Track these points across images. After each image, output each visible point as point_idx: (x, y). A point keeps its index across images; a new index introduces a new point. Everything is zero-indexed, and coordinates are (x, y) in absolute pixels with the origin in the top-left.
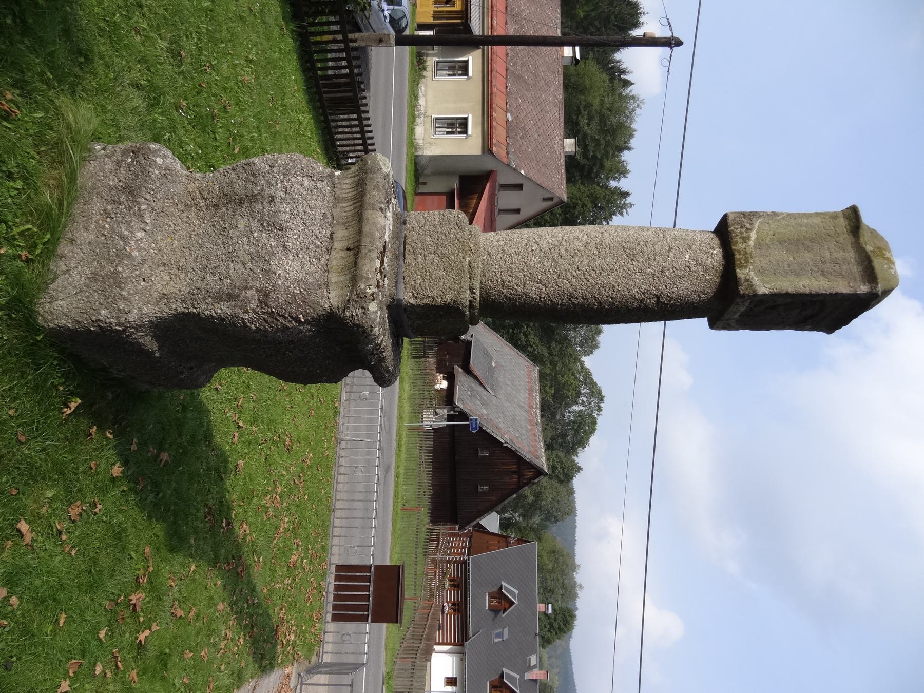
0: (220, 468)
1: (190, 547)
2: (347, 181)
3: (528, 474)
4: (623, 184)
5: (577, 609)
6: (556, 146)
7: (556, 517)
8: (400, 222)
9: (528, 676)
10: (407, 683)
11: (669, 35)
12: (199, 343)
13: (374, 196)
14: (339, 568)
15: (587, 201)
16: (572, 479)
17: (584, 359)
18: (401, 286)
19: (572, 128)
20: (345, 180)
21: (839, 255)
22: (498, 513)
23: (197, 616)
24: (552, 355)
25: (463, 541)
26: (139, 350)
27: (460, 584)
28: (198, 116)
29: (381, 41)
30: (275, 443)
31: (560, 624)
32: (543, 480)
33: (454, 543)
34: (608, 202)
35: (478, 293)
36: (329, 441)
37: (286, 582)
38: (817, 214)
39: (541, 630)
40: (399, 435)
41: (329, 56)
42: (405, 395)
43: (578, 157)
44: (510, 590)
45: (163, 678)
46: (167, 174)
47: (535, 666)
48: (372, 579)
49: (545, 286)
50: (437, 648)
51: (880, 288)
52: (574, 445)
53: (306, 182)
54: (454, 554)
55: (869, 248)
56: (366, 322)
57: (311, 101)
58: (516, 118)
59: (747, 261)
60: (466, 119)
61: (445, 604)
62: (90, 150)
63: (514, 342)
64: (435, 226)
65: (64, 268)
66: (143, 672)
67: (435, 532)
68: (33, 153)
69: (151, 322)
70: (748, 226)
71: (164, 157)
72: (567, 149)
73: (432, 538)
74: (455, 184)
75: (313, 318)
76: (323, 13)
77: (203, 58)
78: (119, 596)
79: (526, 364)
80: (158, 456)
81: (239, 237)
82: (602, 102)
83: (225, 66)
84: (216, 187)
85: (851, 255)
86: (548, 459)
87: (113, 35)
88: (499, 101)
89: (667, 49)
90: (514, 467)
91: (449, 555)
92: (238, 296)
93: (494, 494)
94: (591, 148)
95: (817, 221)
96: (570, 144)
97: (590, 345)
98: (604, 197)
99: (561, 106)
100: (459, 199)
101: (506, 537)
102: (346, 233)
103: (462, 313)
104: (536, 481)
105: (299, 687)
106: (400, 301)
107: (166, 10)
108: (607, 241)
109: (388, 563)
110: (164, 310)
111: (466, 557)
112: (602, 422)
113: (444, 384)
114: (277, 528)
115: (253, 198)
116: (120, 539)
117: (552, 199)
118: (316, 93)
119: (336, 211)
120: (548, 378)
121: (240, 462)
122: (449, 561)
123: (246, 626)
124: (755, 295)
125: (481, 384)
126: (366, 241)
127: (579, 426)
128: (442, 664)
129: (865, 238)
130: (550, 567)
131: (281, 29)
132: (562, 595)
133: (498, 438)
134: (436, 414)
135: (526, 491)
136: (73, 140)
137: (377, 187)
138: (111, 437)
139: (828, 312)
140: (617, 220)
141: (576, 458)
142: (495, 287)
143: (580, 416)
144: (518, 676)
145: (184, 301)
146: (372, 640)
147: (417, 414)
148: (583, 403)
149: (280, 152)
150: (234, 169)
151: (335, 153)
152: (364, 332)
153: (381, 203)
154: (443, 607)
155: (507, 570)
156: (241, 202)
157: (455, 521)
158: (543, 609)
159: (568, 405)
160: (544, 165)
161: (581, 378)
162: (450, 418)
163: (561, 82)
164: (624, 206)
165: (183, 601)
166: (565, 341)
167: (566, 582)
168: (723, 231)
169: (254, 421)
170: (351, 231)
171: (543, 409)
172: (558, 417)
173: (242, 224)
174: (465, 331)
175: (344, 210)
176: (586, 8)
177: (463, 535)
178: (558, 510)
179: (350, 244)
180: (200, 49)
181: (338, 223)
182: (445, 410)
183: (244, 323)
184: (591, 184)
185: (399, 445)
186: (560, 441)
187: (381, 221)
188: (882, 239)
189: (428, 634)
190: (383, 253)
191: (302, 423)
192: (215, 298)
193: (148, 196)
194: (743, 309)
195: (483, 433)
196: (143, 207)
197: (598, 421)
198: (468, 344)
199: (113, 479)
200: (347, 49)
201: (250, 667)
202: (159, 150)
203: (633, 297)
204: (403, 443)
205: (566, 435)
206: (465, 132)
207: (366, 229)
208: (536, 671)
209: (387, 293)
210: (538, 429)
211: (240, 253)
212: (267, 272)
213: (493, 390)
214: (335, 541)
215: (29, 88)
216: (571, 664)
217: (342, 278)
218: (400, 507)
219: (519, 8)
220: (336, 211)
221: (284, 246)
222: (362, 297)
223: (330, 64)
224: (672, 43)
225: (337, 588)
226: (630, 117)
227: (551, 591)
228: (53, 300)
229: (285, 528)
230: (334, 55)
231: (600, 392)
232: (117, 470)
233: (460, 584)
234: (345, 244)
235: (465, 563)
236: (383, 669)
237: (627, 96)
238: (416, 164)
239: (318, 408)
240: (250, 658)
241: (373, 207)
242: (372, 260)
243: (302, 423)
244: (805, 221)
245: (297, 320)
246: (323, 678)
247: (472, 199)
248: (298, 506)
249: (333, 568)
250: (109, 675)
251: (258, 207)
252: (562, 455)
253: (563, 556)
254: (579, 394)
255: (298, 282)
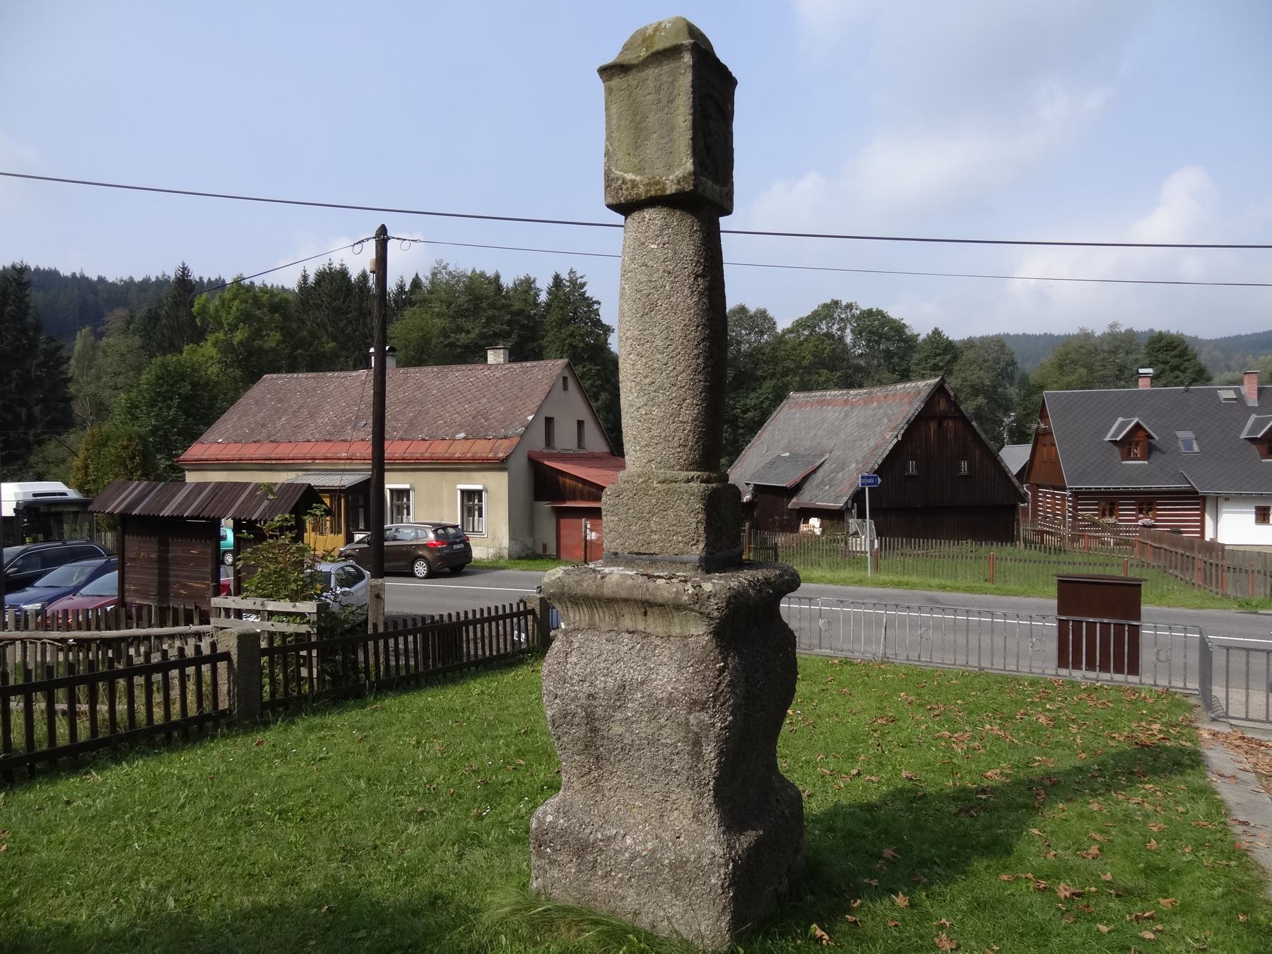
0: (912, 797)
1: (1007, 834)
2: (571, 615)
3: (943, 405)
4: (543, 284)
5: (1151, 330)
6: (498, 375)
7: (1008, 364)
8: (615, 558)
9: (1253, 401)
10: (1261, 577)
11: (373, 243)
12: (747, 783)
13: (588, 585)
14: (1062, 663)
15: (566, 332)
16: (951, 342)
17: (779, 330)
18: (685, 557)
19: (473, 354)
20: (566, 619)
21: (651, 84)
22: (1002, 446)
23: (1102, 832)
24: (774, 375)
25: (1044, 496)
26: (755, 851)
27: (1110, 502)
28: (487, 799)
29: (378, 596)
30: (883, 735)
31: (1172, 356)
32: (953, 383)
33: (1048, 510)
34: (567, 302)
35: (692, 473)
36: (885, 672)
37: (1075, 731)
38: (607, 109)
39: (1182, 384)
40: (884, 584)
41: (393, 663)
42: (829, 575)
43: (509, 345)
44: (1117, 429)
45: (1178, 873)
46: (561, 811)
47: (1238, 391)
48: (1077, 619)
49: (684, 400)
50: (1209, 536)
51: (687, 41)
52: (903, 341)
53: (573, 659)
54: (1063, 510)
55: (644, 53)
56: (724, 594)
57: (454, 682)
58: (461, 427)
59: (658, 183)
60: (463, 492)
61: (1140, 523)
62: (538, 894)
63: (755, 426)
64: (620, 520)
65: (666, 923)
66: (1164, 892)
67: (1030, 536)
68: (543, 947)
69: (724, 833)
70: (620, 182)
71: (545, 813)
72: (501, 360)
73: (1038, 541)
74: (546, 506)
75: (720, 653)
76: (356, 661)
77: (421, 790)
78: (1058, 909)
79: (785, 409)
80: (887, 860)
81: (632, 733)
82: (440, 315)
83: (428, 770)
84: (577, 758)
85: (651, 72)
86: (923, 377)
87: (412, 872)
88: (440, 449)
89: (390, 243)
90: (933, 426)
91: (1064, 517)
92: (696, 734)
93: (969, 451)
94: (498, 327)
95: (614, 109)
96: (495, 357)
97: (761, 321)
98: (562, 308)
99: (446, 369)
100: (564, 501)
101: (1037, 435)
102: (627, 617)
103: (715, 491)
104: (952, 394)
105: (1233, 722)
106: (701, 560)
107: (375, 823)
108: (637, 333)
109: (1055, 602)
110: (712, 817)
111: (1068, 493)
112: (865, 303)
113: (815, 522)
114: (998, 738)
115: (590, 717)
116: (986, 903)
117: (565, 379)
118: (444, 675)
119: (604, 627)
120: (807, 379)
121: (904, 774)
122: (1074, 517)
123: (1128, 780)
124: (695, 173)
125: (814, 471)
126: (637, 594)
127: (875, 334)
128: (1235, 528)
129: (631, 58)
130: (1083, 371)
131: (375, 710)
132: (1127, 353)
133: (891, 447)
134: (856, 534)
135: (968, 407)
136: (527, 909)
137: (578, 583)
138: (859, 901)
139: (713, 89)
140: (608, 315)
141: (921, 338)
142: (686, 455)
143: (860, 333)
144: (1254, 417)
145: (701, 795)
146: (1166, 625)
147: (856, 560)
148: (842, 329)
149: (540, 689)
150: (559, 738)
151: (514, 655)
152: (735, 597)
153: (595, 578)
154: (1144, 526)
155: (1087, 435)
156: (595, 730)
157: (1013, 508)
158: (1148, 381)
159: (845, 349)
160: (521, 389)
161: (806, 333)
162: (861, 515)
163: (417, 369)
164: (573, 282)
165: (1079, 848)
166: (755, 355)
167: (1106, 347)
168: (626, 208)
169: (852, 757)
170: (626, 610)
171: (850, 386)
172: (862, 363)
173: (617, 729)
174: (736, 492)
175: (603, 618)
176: (324, 339)
177: (1035, 497)
178: (997, 361)
179: (639, 611)
180: (412, 793)
181: (617, 625)
182: (851, 521)
183: (725, 728)
184: (548, 326)
185: (898, 585)
186: (896, 360)
187: (615, 578)
188: (633, 37)
189: (1184, 547)
190: (649, 577)
191: (857, 705)
192: (698, 759)
193: (588, 831)
194: (710, 183)
195: (882, 469)
196: (599, 836)
197: (865, 308)
198: (759, 489)
199: (912, 905)
200: (386, 636)
201: (1189, 779)
202: (538, 818)
203: (697, 303)
204: (895, 579)
205: (887, 352)
206: (479, 493)
207: (624, 594)
208: (1244, 389)
209: (693, 573)
210: (878, 391)
211: (650, 731)
212: (670, 702)
213: (822, 455)
214: (1024, 669)
215: (477, 947)
216: (1239, 337)
217: (677, 621)
218: (988, 585)
219: (327, 424)
220: (604, 627)
221: (642, 683)
222: (698, 598)
223: (402, 662)
224: (382, 238)
225: (1091, 667)
226: (456, 277)
227: (1122, 369)
228: (700, 936)
229: (1000, 729)
230: (392, 658)
231: (825, 306)
232: (901, 900)
233: (1110, 502)
234: (640, 618)
235: (1077, 494)
236: (1234, 612)
237: (432, 283)
238: (519, 558)
239: (840, 683)
240: (1178, 778)
241: (600, 587)
242: (657, 588)
243: (857, 705)
244: (614, 121)
245: (722, 670)
246: (1218, 691)
247: (564, 484)
248: (971, 712)
249: (1064, 672)
250: (1160, 927)
251: (599, 711)
252: (916, 357)
253: (1067, 353)
254: (829, 335)
255: (680, 668)
